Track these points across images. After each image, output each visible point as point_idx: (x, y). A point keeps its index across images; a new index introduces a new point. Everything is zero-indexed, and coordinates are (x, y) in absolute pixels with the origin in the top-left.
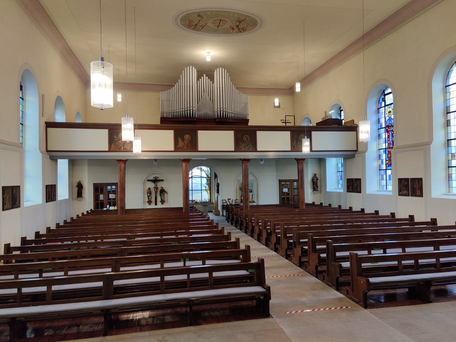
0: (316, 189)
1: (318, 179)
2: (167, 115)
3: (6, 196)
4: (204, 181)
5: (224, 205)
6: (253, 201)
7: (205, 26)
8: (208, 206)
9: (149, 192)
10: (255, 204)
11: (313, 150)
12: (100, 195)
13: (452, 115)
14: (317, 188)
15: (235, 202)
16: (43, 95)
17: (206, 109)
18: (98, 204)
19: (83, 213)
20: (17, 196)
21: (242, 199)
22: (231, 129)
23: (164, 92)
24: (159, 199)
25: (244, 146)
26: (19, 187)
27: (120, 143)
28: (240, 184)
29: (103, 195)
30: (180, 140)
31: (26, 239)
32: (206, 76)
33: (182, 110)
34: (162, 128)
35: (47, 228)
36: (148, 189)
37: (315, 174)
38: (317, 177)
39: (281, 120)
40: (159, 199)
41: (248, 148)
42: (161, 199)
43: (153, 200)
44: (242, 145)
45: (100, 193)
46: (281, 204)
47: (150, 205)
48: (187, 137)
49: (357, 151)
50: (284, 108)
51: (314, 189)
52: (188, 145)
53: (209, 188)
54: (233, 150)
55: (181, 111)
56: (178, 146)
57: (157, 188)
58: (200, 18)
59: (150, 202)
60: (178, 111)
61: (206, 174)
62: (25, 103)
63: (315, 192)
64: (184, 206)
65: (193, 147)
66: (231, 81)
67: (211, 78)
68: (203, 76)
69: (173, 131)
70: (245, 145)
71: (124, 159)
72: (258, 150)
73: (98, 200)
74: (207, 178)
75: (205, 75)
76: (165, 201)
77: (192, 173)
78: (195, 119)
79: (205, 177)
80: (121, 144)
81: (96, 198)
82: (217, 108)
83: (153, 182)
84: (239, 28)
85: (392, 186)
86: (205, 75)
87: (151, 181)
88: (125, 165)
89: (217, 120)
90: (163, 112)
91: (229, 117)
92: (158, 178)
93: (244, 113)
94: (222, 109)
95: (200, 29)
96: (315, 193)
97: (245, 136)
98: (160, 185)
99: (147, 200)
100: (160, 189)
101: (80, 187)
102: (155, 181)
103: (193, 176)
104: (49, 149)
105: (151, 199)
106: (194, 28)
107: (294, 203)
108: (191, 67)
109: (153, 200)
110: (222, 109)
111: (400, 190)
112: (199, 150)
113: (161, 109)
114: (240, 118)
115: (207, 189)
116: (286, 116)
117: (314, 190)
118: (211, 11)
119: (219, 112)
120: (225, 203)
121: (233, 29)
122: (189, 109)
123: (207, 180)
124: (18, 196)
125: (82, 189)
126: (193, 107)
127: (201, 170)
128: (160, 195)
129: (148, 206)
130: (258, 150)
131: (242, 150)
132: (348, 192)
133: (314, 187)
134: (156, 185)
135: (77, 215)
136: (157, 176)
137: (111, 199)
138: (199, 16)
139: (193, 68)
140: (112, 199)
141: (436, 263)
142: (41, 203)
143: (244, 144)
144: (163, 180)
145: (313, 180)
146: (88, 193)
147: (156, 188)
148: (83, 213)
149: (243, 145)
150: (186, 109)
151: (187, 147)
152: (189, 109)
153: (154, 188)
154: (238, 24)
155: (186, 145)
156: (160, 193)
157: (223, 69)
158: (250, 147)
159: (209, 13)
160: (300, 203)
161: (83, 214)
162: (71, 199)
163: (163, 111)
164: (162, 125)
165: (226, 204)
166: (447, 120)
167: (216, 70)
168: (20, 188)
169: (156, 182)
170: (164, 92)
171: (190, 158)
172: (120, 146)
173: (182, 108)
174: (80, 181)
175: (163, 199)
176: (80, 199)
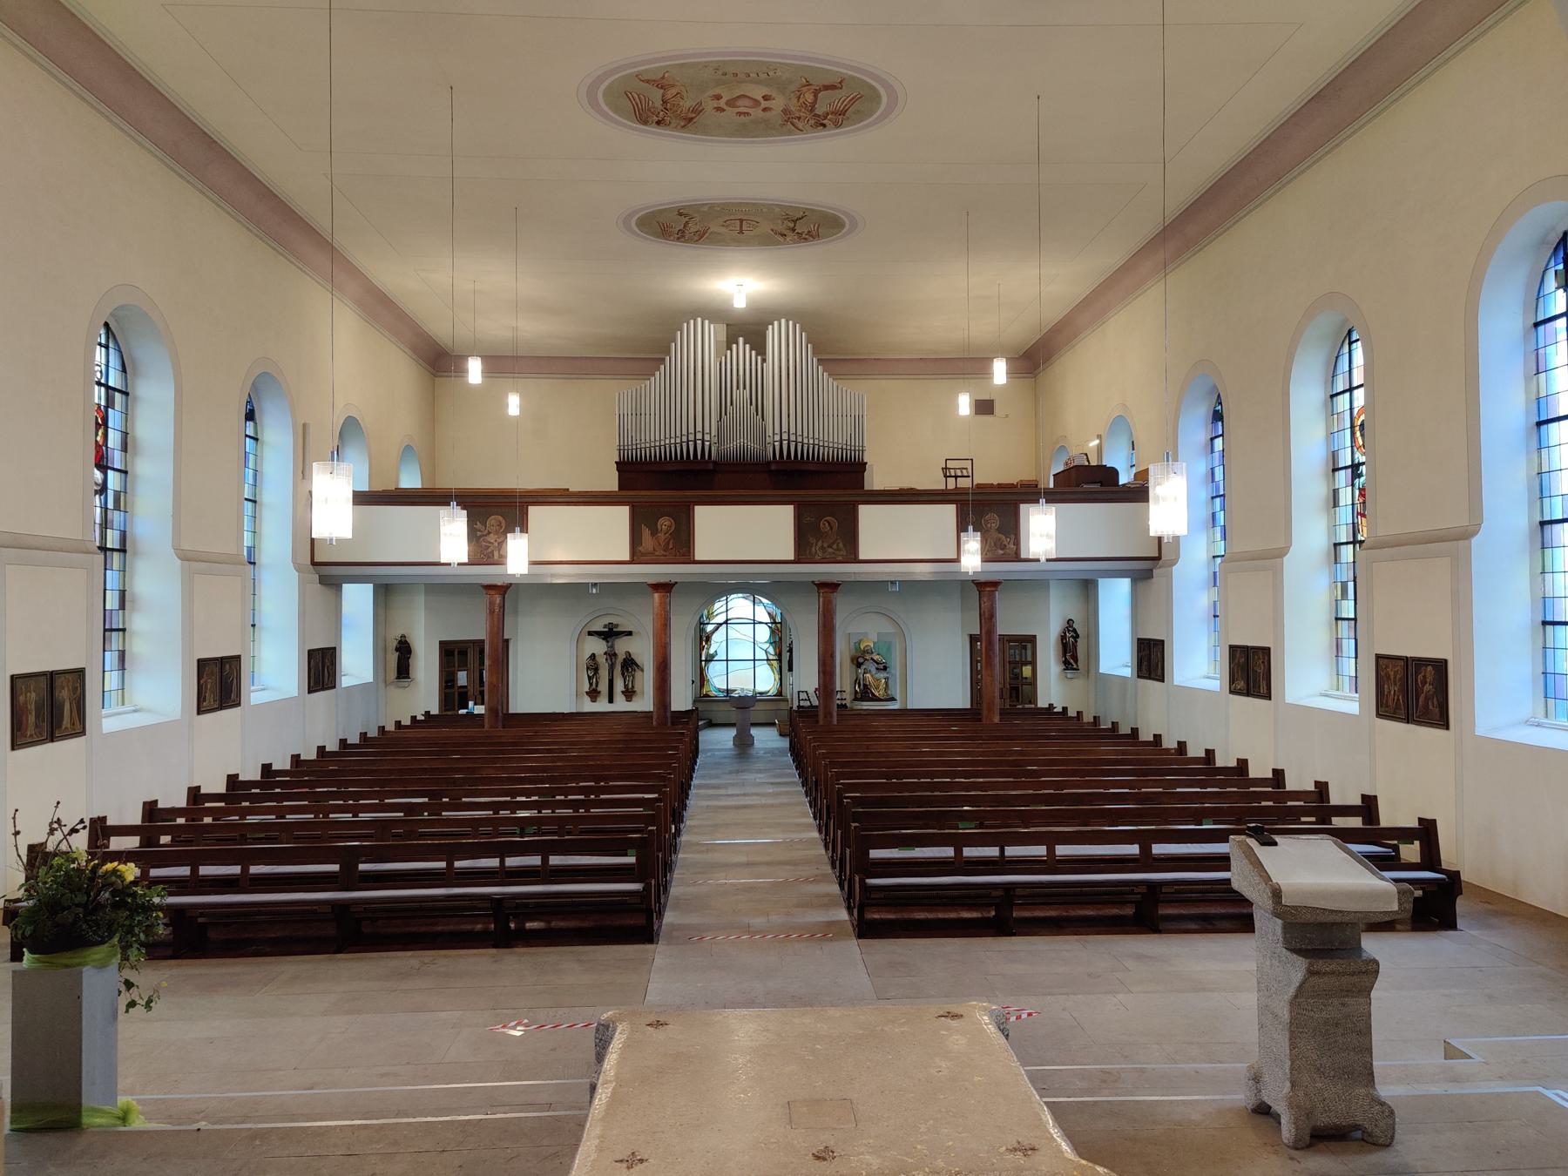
1: (1078, 636)
3: (206, 682)
4: (764, 633)
5: (803, 707)
6: (888, 695)
7: (704, 234)
8: (752, 709)
9: (593, 666)
12: (459, 673)
13: (1562, 433)
14: (1076, 661)
16: (304, 425)
18: (452, 695)
19: (400, 722)
21: (856, 691)
22: (786, 499)
24: (619, 686)
25: (822, 548)
26: (238, 657)
27: (490, 543)
30: (646, 533)
31: (238, 778)
33: (662, 443)
34: (598, 500)
36: (591, 657)
38: (1075, 631)
40: (619, 686)
41: (834, 553)
42: (626, 686)
43: (603, 687)
45: (459, 666)
46: (975, 707)
47: (630, 701)
48: (665, 523)
49: (1159, 558)
50: (1007, 416)
51: (1065, 665)
53: (776, 654)
54: (792, 558)
55: (670, 444)
56: (640, 548)
57: (615, 655)
58: (687, 219)
59: (593, 694)
60: (662, 443)
61: (769, 614)
63: (1070, 674)
64: (821, 701)
67: (759, 347)
68: (737, 344)
69: (627, 508)
70: (825, 545)
71: (499, 584)
72: (861, 557)
73: (453, 686)
74: (770, 625)
75: (741, 340)
76: (635, 692)
78: (711, 467)
79: (766, 624)
80: (493, 543)
81: (447, 681)
82: (771, 435)
83: (603, 639)
84: (798, 233)
85: (838, 689)
86: (741, 340)
87: (598, 634)
88: (504, 597)
89: (773, 467)
90: (622, 448)
91: (823, 459)
92: (617, 626)
93: (853, 444)
95: (696, 238)
98: (622, 646)
99: (586, 688)
100: (621, 657)
101: (404, 650)
102: (610, 634)
105: (597, 686)
106: (678, 238)
107: (1010, 705)
108: (699, 320)
109: (603, 687)
110: (785, 436)
111: (1232, 680)
112: (697, 558)
113: (617, 441)
115: (771, 657)
116: (946, 460)
119: (777, 444)
122: (701, 438)
123: (773, 632)
124: (235, 679)
125: (409, 658)
126: (705, 432)
127: (754, 601)
128: (623, 674)
129: (589, 706)
130: (861, 557)
131: (817, 558)
132: (1139, 677)
133: (1066, 659)
134: (612, 647)
135: (396, 722)
136: (614, 620)
138: (681, 214)
139: (707, 322)
142: (372, 680)
144: (630, 633)
145: (1063, 637)
146: (427, 666)
147: (611, 655)
148: (400, 722)
149: (820, 543)
150: (684, 439)
151: (665, 551)
152: (691, 437)
153: (605, 653)
154: (792, 225)
155: (663, 544)
156: (622, 667)
157: (791, 322)
158: (838, 549)
159: (706, 209)
160: (985, 706)
161: (398, 724)
162: (382, 685)
163: (622, 444)
165: (808, 704)
166: (1334, 490)
167: (770, 327)
168: (240, 661)
169: (611, 636)
171: (673, 581)
172: (490, 550)
173: (673, 435)
174: (403, 636)
175: (630, 686)
176: (404, 682)
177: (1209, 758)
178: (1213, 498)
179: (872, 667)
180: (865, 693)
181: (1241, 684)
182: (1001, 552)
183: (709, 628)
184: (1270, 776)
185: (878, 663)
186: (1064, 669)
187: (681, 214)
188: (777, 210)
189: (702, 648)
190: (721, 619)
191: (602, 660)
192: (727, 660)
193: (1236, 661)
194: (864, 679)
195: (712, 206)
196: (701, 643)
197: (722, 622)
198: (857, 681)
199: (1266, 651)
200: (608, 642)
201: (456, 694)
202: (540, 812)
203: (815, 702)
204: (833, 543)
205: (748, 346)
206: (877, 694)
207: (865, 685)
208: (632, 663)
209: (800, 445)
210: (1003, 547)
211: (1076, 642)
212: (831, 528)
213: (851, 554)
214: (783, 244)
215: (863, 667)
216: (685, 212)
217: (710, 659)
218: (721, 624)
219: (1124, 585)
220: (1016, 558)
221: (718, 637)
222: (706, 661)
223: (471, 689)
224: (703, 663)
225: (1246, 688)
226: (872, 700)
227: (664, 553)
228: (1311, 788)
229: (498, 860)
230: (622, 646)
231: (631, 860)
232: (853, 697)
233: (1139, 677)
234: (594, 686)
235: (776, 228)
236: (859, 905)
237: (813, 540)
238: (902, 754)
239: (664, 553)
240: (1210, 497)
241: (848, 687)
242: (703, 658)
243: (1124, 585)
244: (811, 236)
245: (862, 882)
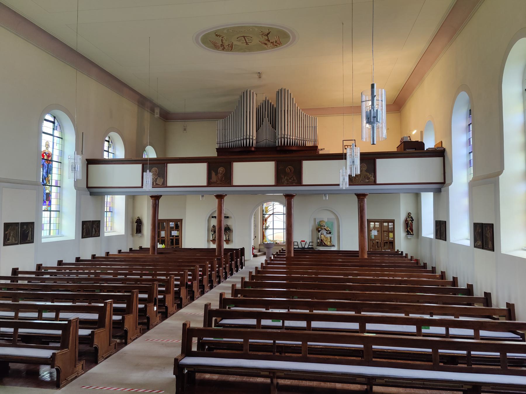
0: (410, 233)
1: (413, 220)
8: (272, 248)
10: (333, 249)
12: (162, 232)
14: (412, 231)
15: (309, 245)
17: (266, 137)
20: (29, 232)
23: (223, 119)
24: (224, 238)
25: (287, 179)
26: (33, 223)
28: (317, 223)
29: (164, 231)
30: (213, 174)
35: (37, 265)
37: (409, 214)
38: (412, 218)
44: (284, 178)
49: (444, 183)
52: (222, 179)
62: (64, 142)
63: (409, 236)
65: (227, 181)
70: (288, 178)
72: (168, 185)
77: (273, 209)
78: (253, 149)
84: (271, 42)
89: (278, 149)
91: (299, 145)
96: (409, 237)
101: (139, 223)
103: (274, 213)
104: (89, 186)
111: (475, 240)
114: (240, 145)
117: (408, 234)
118: (226, 28)
120: (296, 245)
121: (266, 44)
137: (173, 236)
140: (174, 237)
141: (499, 357)
143: (286, 177)
145: (406, 220)
149: (286, 177)
164: (219, 157)
165: (297, 247)
177: (454, 281)
178: (470, 153)
179: (324, 232)
180: (321, 243)
181: (479, 243)
182: (367, 181)
183: (266, 216)
184: (483, 296)
185: (327, 231)
186: (407, 235)
187: (217, 35)
188: (256, 29)
189: (263, 224)
190: (271, 212)
192: (273, 229)
193: (477, 230)
195: (228, 29)
196: (263, 222)
197: (271, 214)
198: (318, 238)
199: (491, 226)
206: (326, 243)
207: (321, 240)
208: (229, 229)
209: (294, 140)
210: (369, 179)
211: (413, 223)
212: (291, 171)
213: (299, 183)
214: (266, 49)
215: (321, 232)
216: (218, 34)
218: (271, 215)
219: (431, 195)
220: (375, 183)
221: (270, 220)
222: (265, 229)
223: (166, 238)
224: (264, 230)
225: (481, 245)
226: (324, 246)
227: (221, 182)
228: (504, 307)
232: (317, 245)
233: (436, 238)
237: (283, 176)
238: (399, 263)
239: (221, 182)
240: (469, 153)
242: (264, 228)
243: (431, 195)
244: (276, 44)
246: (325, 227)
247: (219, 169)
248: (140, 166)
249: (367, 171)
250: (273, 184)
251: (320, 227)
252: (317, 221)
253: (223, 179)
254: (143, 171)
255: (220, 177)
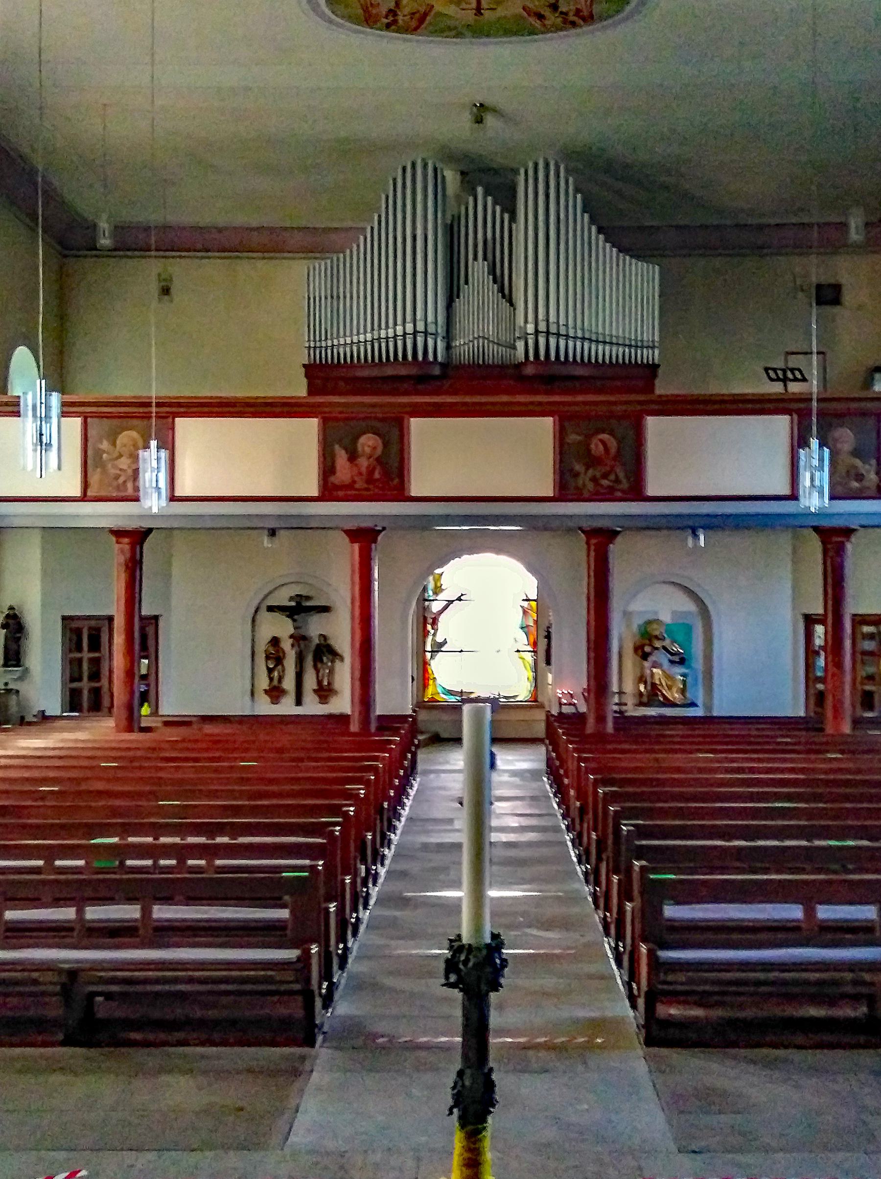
2: (323, 356)
10: (698, 712)
11: (178, 493)
24: (310, 682)
32: (487, 193)
39: (766, 370)
40: (310, 682)
42: (319, 683)
43: (289, 683)
47: (326, 703)
66: (584, 211)
70: (598, 475)
72: (651, 491)
75: (480, 190)
78: (437, 371)
83: (288, 616)
84: (562, 13)
86: (480, 190)
89: (529, 370)
92: (308, 598)
94: (555, 326)
97: (601, 441)
98: (315, 627)
99: (263, 683)
112: (413, 494)
121: (540, 17)
129: (265, 707)
130: (651, 491)
144: (325, 609)
147: (299, 639)
153: (291, 636)
170: (323, 263)
175: (326, 683)
179: (663, 658)
180: (653, 696)
185: (672, 654)
189: (426, 634)
191: (287, 645)
194: (652, 674)
196: (425, 627)
198: (642, 679)
200: (294, 621)
201: (85, 693)
202: (156, 839)
203: (583, 709)
204: (609, 473)
205: (490, 199)
207: (654, 685)
215: (652, 658)
217: (438, 647)
229: (155, 915)
230: (315, 627)
231: (284, 914)
234: (275, 682)
235: (531, 5)
236: (647, 993)
241: (629, 687)
242: (428, 648)
245: (651, 953)
246: (667, 643)
247: (363, 440)
248: (781, 424)
249: (856, 453)
250: (315, 493)
251: (647, 642)
252: (637, 622)
253: (377, 475)
254: (800, 441)
255: (364, 470)
